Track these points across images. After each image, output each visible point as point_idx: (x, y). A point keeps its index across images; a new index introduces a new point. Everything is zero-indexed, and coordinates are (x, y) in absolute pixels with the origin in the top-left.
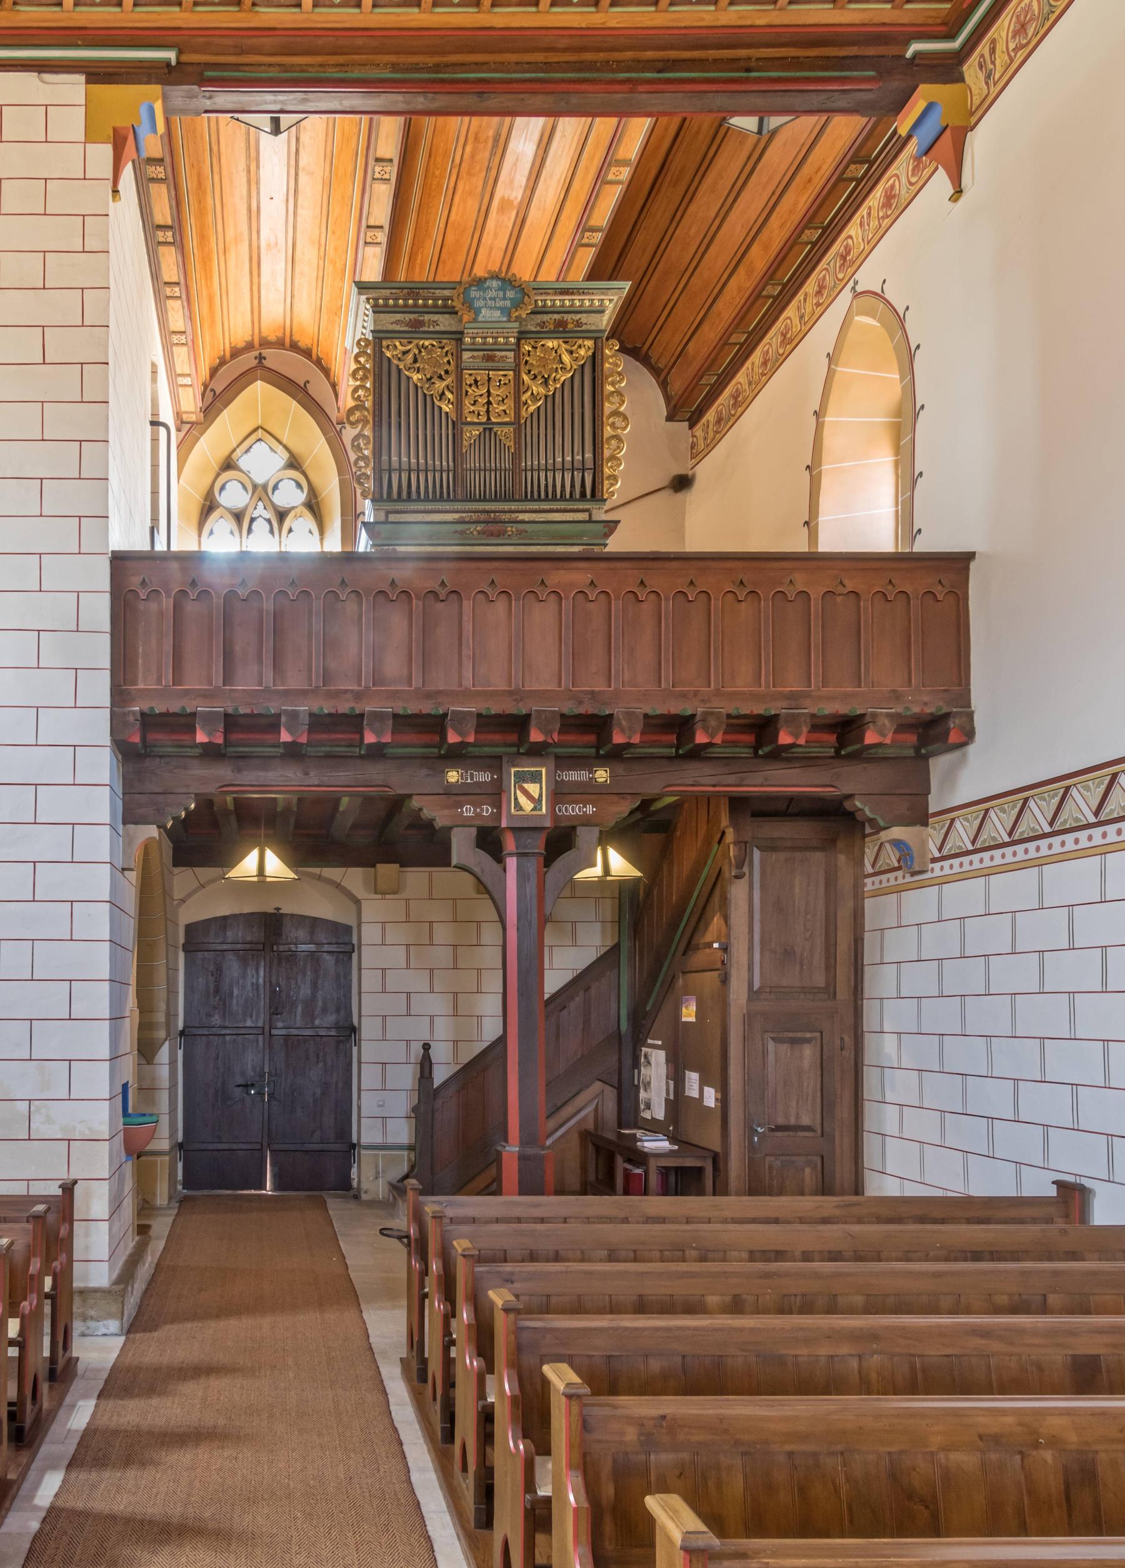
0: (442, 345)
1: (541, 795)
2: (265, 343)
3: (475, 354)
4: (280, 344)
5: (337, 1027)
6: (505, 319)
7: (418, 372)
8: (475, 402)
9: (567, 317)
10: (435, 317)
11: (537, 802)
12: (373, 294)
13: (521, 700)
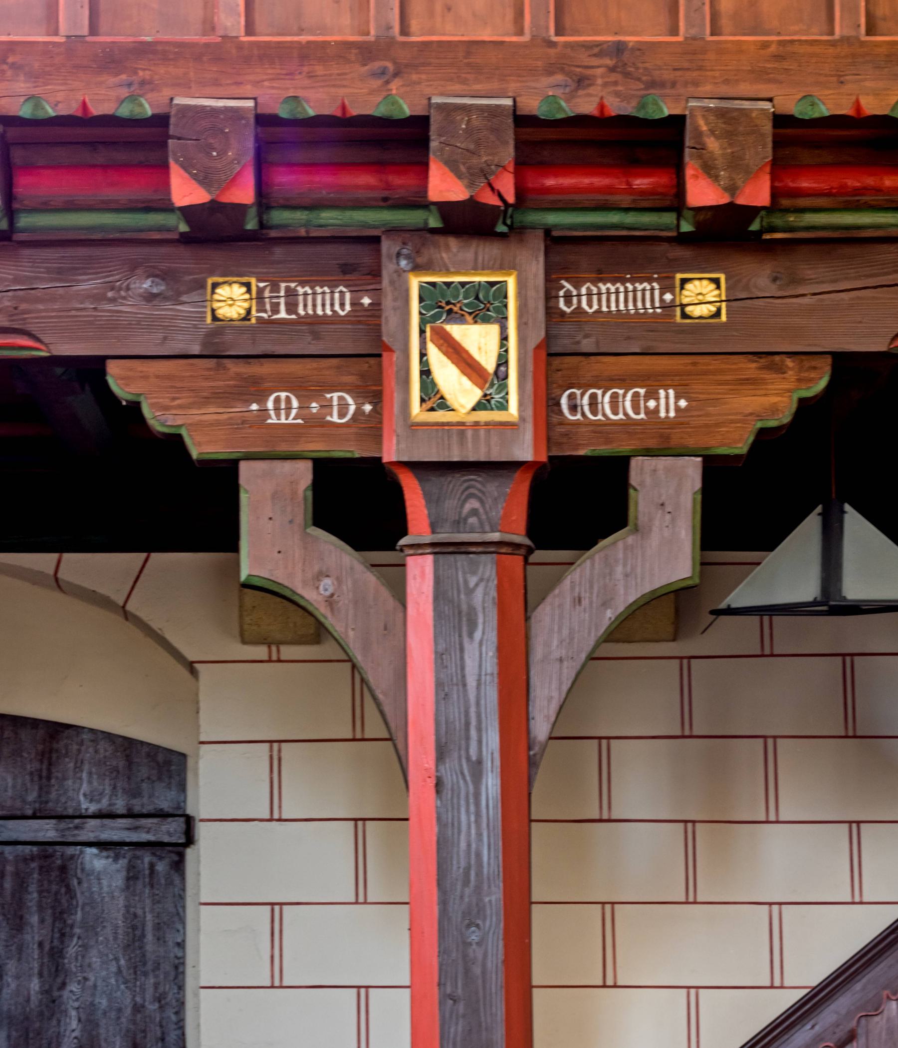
1: (502, 361)
13: (396, 74)
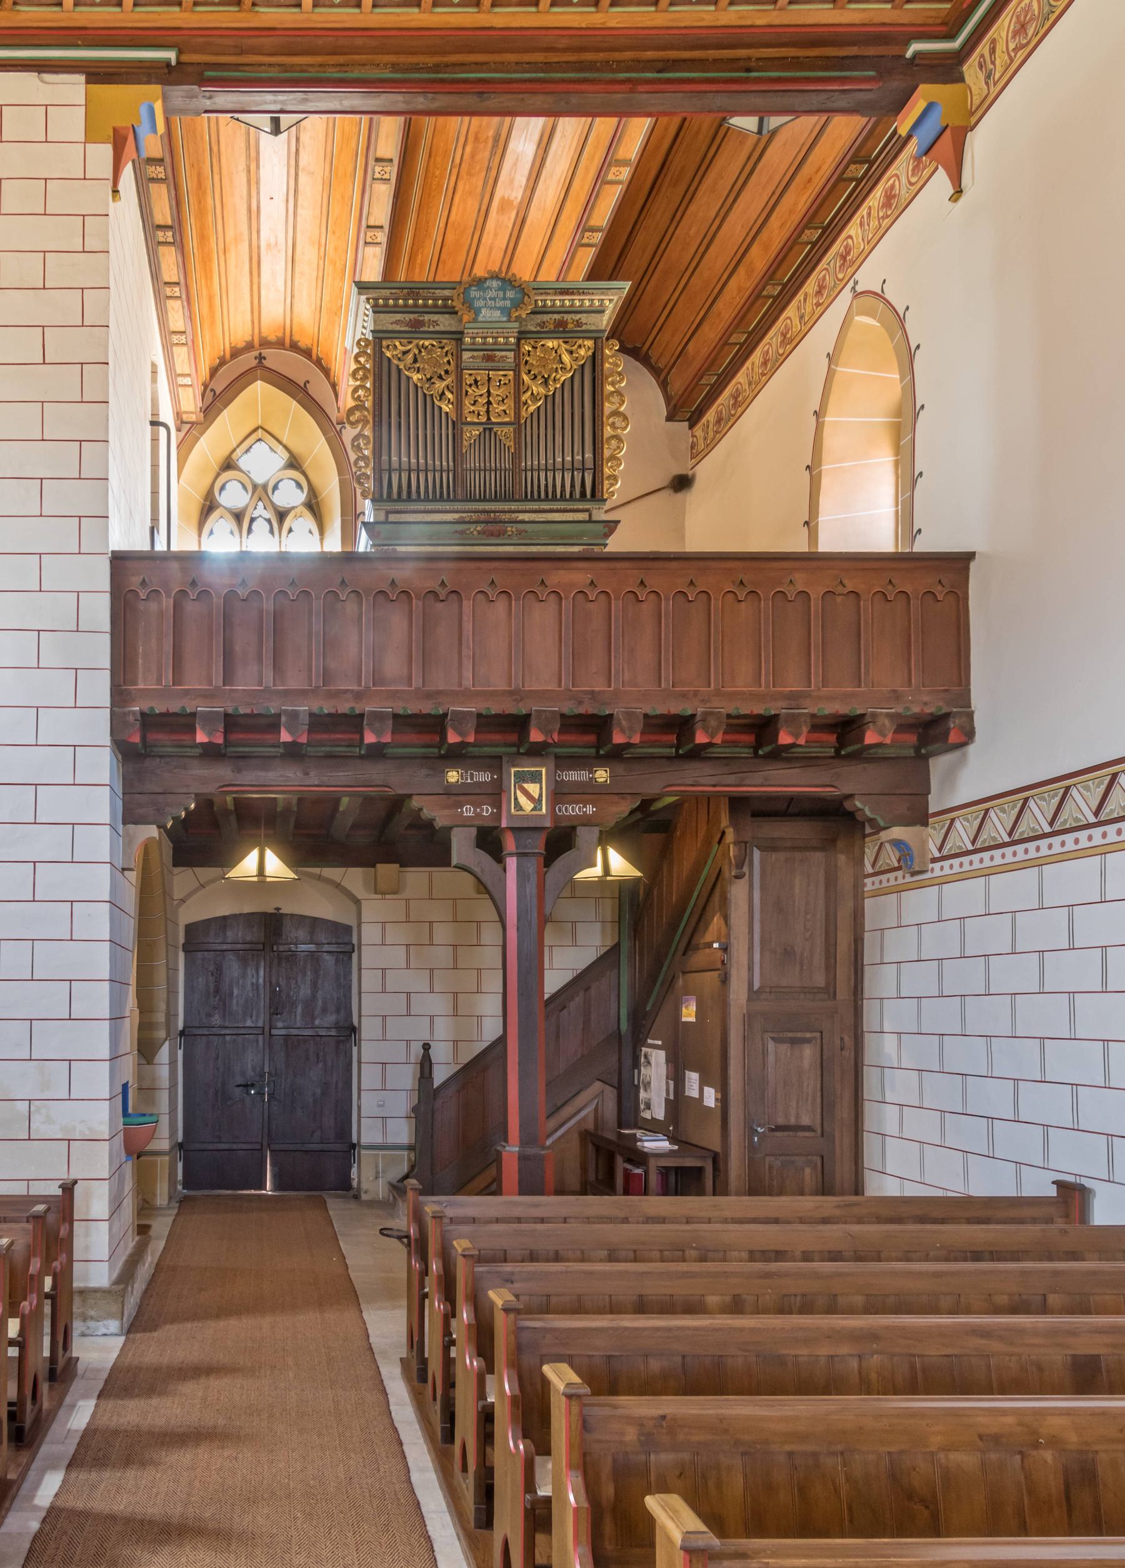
0: (442, 345)
1: (541, 795)
2: (265, 343)
3: (475, 354)
4: (280, 344)
5: (337, 1027)
6: (505, 319)
7: (418, 372)
8: (475, 402)
9: (566, 316)
10: (435, 317)
11: (537, 802)
12: (373, 294)
13: (521, 700)
